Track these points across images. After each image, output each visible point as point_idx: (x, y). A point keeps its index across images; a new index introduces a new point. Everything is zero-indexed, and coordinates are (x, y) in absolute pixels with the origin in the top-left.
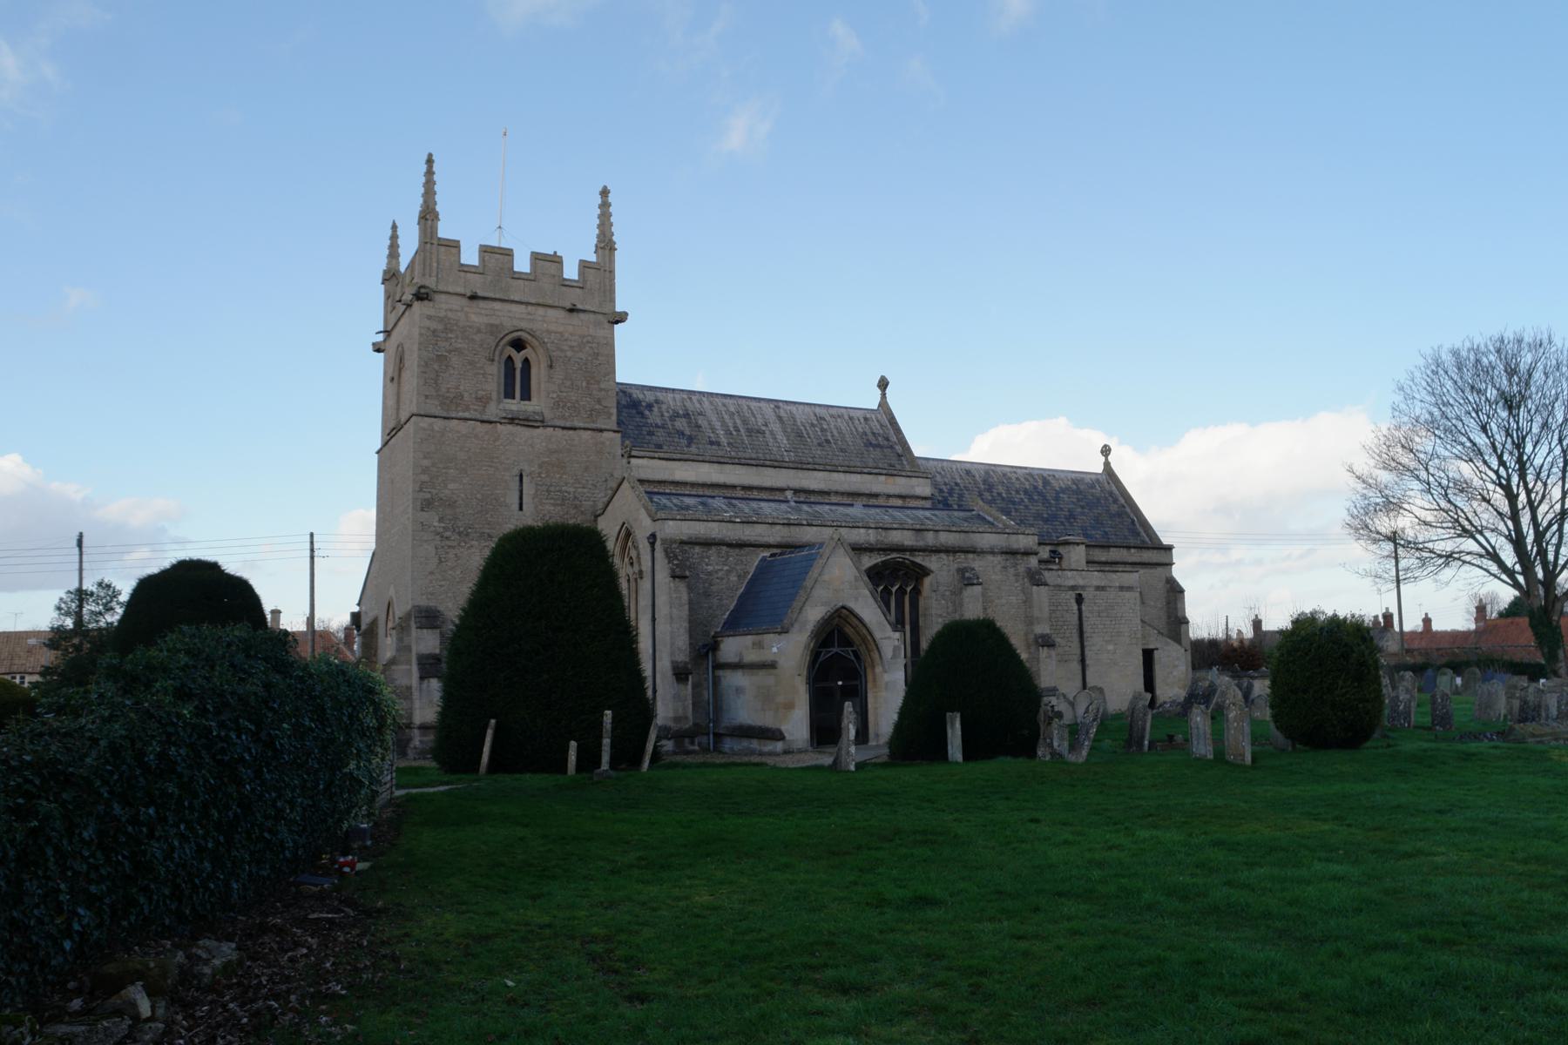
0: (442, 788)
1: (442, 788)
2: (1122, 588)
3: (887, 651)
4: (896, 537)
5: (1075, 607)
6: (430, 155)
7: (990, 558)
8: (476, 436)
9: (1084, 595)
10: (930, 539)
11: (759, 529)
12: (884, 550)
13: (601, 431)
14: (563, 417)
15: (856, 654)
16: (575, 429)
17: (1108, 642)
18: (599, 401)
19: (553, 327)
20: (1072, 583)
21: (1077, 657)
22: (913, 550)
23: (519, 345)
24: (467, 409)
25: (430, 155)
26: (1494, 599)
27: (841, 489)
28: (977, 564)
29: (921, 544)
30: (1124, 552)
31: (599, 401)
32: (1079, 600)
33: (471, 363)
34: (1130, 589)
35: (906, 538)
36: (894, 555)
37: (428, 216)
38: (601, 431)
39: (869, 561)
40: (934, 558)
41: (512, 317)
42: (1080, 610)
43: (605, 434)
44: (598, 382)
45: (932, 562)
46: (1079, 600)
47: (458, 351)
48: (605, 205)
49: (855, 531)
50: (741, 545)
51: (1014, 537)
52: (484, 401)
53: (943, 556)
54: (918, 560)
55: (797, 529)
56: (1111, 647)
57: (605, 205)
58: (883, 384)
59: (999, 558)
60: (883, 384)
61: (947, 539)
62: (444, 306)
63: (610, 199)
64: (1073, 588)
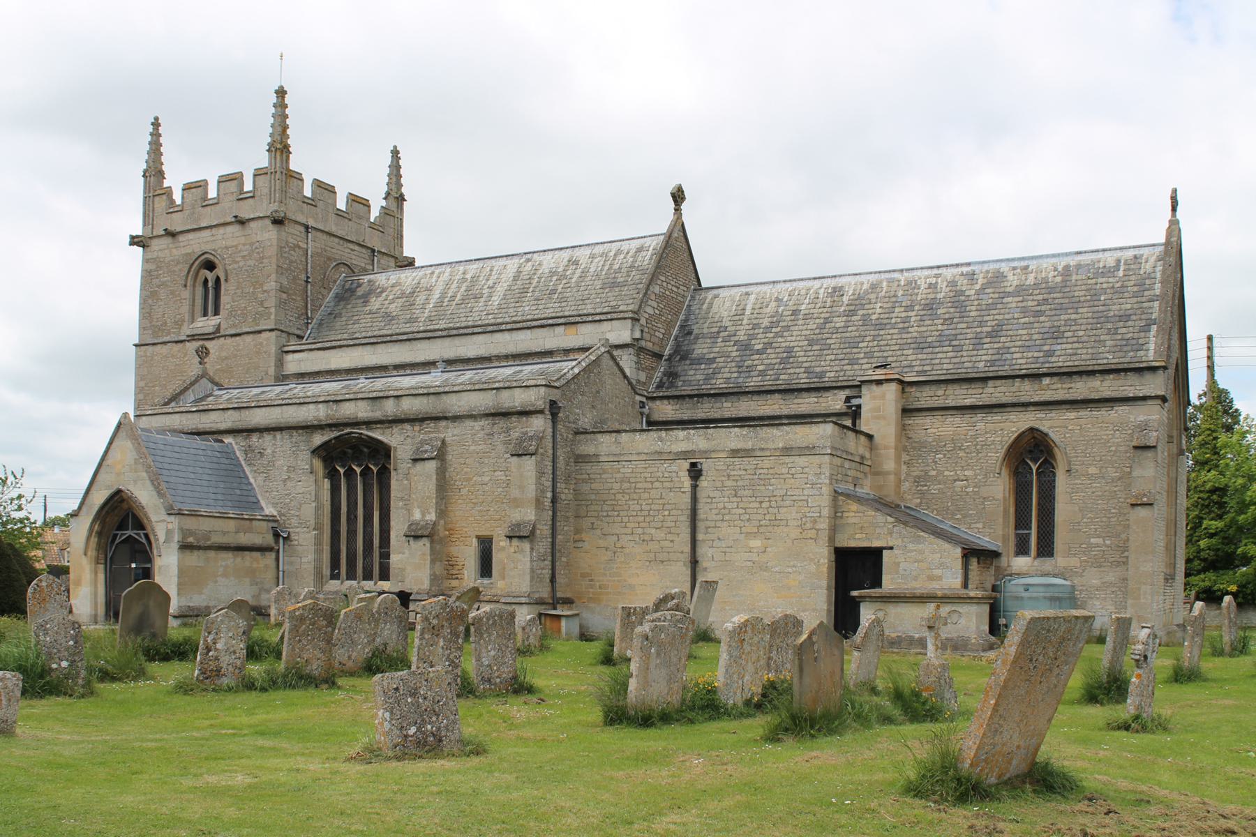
2: (787, 451)
3: (161, 535)
4: (350, 410)
5: (687, 483)
6: (157, 119)
7: (469, 423)
8: (173, 356)
9: (706, 465)
10: (390, 408)
11: (213, 416)
12: (330, 426)
13: (260, 332)
14: (234, 326)
15: (147, 536)
16: (239, 335)
17: (755, 535)
18: (262, 303)
19: (229, 243)
21: (687, 556)
22: (368, 423)
23: (210, 266)
24: (169, 333)
25: (157, 119)
27: (504, 351)
28: (450, 432)
29: (378, 415)
30: (1027, 385)
31: (262, 303)
32: (695, 472)
33: (172, 293)
35: (362, 411)
36: (348, 430)
37: (280, 147)
38: (260, 332)
39: (319, 439)
41: (196, 244)
42: (695, 487)
43: (264, 335)
44: (262, 285)
46: (695, 472)
47: (163, 284)
48: (156, 135)
49: (304, 408)
51: (505, 394)
52: (179, 324)
53: (407, 426)
54: (377, 434)
55: (247, 412)
56: (756, 543)
57: (156, 135)
58: (678, 196)
59: (483, 422)
60: (678, 196)
62: (156, 248)
63: (161, 130)
64: (684, 455)
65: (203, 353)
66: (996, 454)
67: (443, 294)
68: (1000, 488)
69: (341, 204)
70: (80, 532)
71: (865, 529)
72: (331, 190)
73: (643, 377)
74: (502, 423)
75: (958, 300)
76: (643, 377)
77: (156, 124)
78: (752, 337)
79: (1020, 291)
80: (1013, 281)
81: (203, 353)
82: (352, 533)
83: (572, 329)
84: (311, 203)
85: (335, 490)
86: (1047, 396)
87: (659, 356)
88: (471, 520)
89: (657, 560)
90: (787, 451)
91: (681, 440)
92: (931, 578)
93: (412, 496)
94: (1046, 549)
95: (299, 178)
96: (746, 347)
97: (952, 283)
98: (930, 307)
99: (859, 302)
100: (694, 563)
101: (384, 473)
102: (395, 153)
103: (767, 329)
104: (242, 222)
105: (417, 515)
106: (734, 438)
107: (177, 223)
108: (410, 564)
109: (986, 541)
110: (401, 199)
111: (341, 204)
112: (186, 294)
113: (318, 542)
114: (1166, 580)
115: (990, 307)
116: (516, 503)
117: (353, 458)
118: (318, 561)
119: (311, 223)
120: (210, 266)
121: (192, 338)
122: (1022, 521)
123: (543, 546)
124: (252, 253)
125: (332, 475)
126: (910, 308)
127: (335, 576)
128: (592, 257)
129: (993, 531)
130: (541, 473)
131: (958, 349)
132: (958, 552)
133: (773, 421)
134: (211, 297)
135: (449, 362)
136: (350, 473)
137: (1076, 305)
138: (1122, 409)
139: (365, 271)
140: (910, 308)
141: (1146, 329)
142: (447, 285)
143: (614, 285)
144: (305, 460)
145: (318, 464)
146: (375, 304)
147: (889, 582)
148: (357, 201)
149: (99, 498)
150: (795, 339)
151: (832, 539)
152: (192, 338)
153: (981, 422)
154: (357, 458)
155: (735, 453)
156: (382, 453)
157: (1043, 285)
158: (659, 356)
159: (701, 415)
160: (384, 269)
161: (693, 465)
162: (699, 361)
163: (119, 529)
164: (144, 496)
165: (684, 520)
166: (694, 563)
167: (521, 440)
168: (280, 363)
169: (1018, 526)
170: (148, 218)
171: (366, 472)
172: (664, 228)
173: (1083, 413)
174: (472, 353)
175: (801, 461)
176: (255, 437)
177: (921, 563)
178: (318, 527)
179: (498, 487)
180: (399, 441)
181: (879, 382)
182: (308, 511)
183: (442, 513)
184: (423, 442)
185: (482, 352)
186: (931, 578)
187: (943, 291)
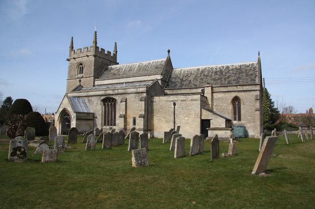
0: (287, 140)
1: (287, 140)
2: (192, 100)
3: (73, 117)
5: (173, 106)
7: (132, 95)
10: (116, 92)
20: (172, 99)
22: (112, 95)
23: (81, 64)
26: (256, 96)
28: (128, 97)
32: (175, 104)
34: (196, 100)
39: (102, 98)
40: (117, 96)
41: (78, 60)
45: (116, 97)
46: (175, 104)
50: (79, 97)
54: (113, 97)
56: (186, 118)
58: (169, 51)
59: (134, 95)
60: (169, 51)
61: (120, 91)
64: (172, 101)
65: (80, 81)
66: (230, 101)
67: (125, 70)
68: (231, 107)
69: (106, 53)
70: (57, 117)
71: (206, 115)
72: (104, 50)
73: (163, 85)
74: (138, 95)
75: (221, 71)
76: (163, 85)
77: (72, 38)
78: (183, 78)
79: (232, 69)
80: (231, 68)
81: (80, 81)
82: (108, 117)
83: (149, 76)
84: (101, 52)
85: (105, 108)
86: (239, 90)
87: (166, 82)
88: (131, 115)
89: (167, 122)
90: (192, 100)
91: (172, 98)
92: (220, 125)
93: (120, 109)
94: (240, 119)
95: (98, 48)
96: (182, 80)
97: (220, 68)
98: (216, 73)
99: (203, 71)
100: (175, 122)
101: (115, 104)
102: (116, 43)
103: (186, 77)
104: (88, 56)
105: (121, 113)
106: (182, 97)
107: (75, 56)
108: (119, 124)
109: (230, 118)
110: (116, 52)
111: (106, 53)
112: (77, 70)
113: (102, 118)
114: (112, 59)
115: (226, 73)
116: (141, 110)
117: (109, 102)
118: (102, 122)
119: (112, 60)
120: (81, 64)
121: (78, 78)
122: (235, 114)
123: (146, 119)
124: (89, 61)
125: (105, 105)
126: (212, 73)
127: (105, 125)
128: (153, 63)
129: (230, 117)
130: (145, 105)
131: (221, 80)
132: (224, 120)
133: (188, 94)
134: (81, 71)
135: (126, 83)
136: (108, 104)
137: (243, 72)
138: (253, 92)
139: (110, 65)
140: (212, 73)
141: (256, 77)
142: (126, 68)
143: (157, 68)
144: (99, 102)
145: (102, 103)
146: (112, 71)
147: (212, 126)
148: (109, 52)
149: (61, 110)
150: (191, 78)
151: (201, 118)
152: (78, 78)
153: (227, 95)
154: (109, 101)
155: (182, 101)
156: (114, 100)
157: (236, 68)
158: (166, 82)
159: (174, 93)
160: (113, 65)
161: (174, 103)
162: (173, 82)
163: (65, 116)
164: (70, 109)
165: (173, 113)
166: (175, 122)
167: (141, 98)
168: (94, 83)
169: (234, 115)
170: (70, 56)
171: (108, 104)
172: (165, 59)
173: (246, 93)
174: (131, 81)
175: (195, 102)
176: (90, 97)
177: (217, 122)
178: (102, 115)
179: (137, 107)
180: (118, 98)
181: (208, 87)
182: (100, 112)
183: (126, 112)
184: (123, 98)
185: (133, 81)
186: (220, 125)
187: (218, 69)
